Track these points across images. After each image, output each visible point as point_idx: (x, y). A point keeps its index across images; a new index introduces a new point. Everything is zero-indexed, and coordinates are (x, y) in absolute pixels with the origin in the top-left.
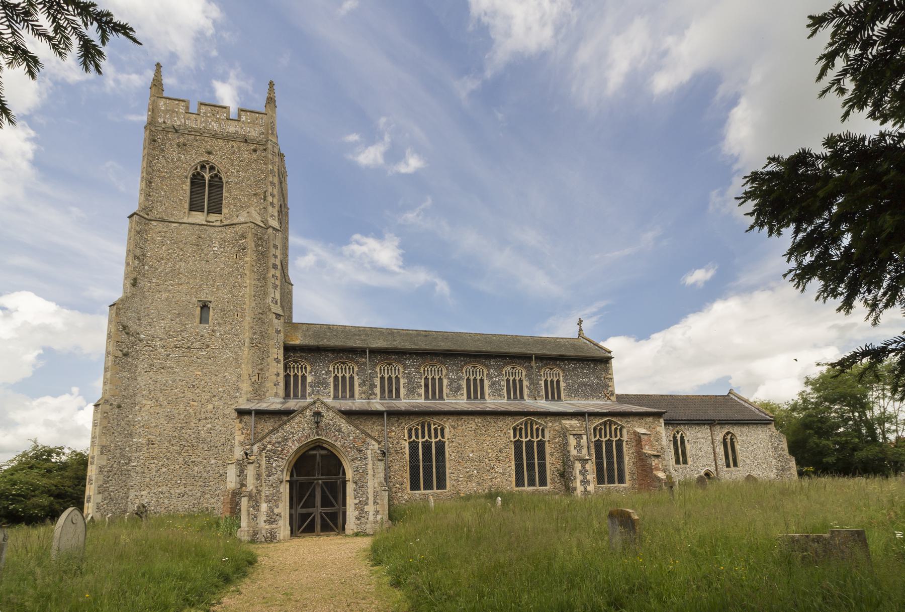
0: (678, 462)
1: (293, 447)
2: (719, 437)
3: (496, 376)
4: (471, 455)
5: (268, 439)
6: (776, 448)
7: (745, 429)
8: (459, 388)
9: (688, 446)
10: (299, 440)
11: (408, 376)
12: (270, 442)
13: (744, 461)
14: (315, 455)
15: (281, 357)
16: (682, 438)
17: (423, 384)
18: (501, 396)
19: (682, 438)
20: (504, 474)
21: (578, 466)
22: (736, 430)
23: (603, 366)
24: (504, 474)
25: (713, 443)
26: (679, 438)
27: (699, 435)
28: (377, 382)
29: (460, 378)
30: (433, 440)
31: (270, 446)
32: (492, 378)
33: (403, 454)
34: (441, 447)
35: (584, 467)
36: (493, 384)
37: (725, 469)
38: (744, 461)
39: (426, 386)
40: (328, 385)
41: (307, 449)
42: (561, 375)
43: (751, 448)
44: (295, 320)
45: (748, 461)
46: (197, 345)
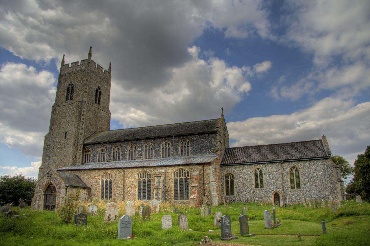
0: (257, 186)
1: (45, 184)
2: (288, 170)
3: (158, 147)
4: (121, 186)
5: (40, 182)
6: (330, 175)
7: (307, 164)
8: (142, 154)
9: (264, 177)
10: (46, 182)
11: (123, 151)
12: (40, 183)
13: (305, 184)
14: (51, 187)
15: (82, 149)
16: (261, 172)
17: (128, 154)
18: (159, 156)
19: (261, 172)
20: (133, 194)
21: (155, 191)
22: (300, 165)
23: (213, 135)
24: (133, 194)
25: (282, 174)
26: (258, 173)
27: (273, 170)
28: (112, 155)
29: (142, 150)
30: (184, 178)
31: (40, 184)
32: (156, 148)
33: (99, 185)
34: (111, 182)
35: (158, 192)
36: (156, 151)
37: (290, 190)
38: (305, 184)
39: (129, 154)
40: (97, 157)
41: (48, 185)
42: (190, 142)
43: (311, 176)
44: (233, 145)
45: (308, 185)
46: (63, 147)
